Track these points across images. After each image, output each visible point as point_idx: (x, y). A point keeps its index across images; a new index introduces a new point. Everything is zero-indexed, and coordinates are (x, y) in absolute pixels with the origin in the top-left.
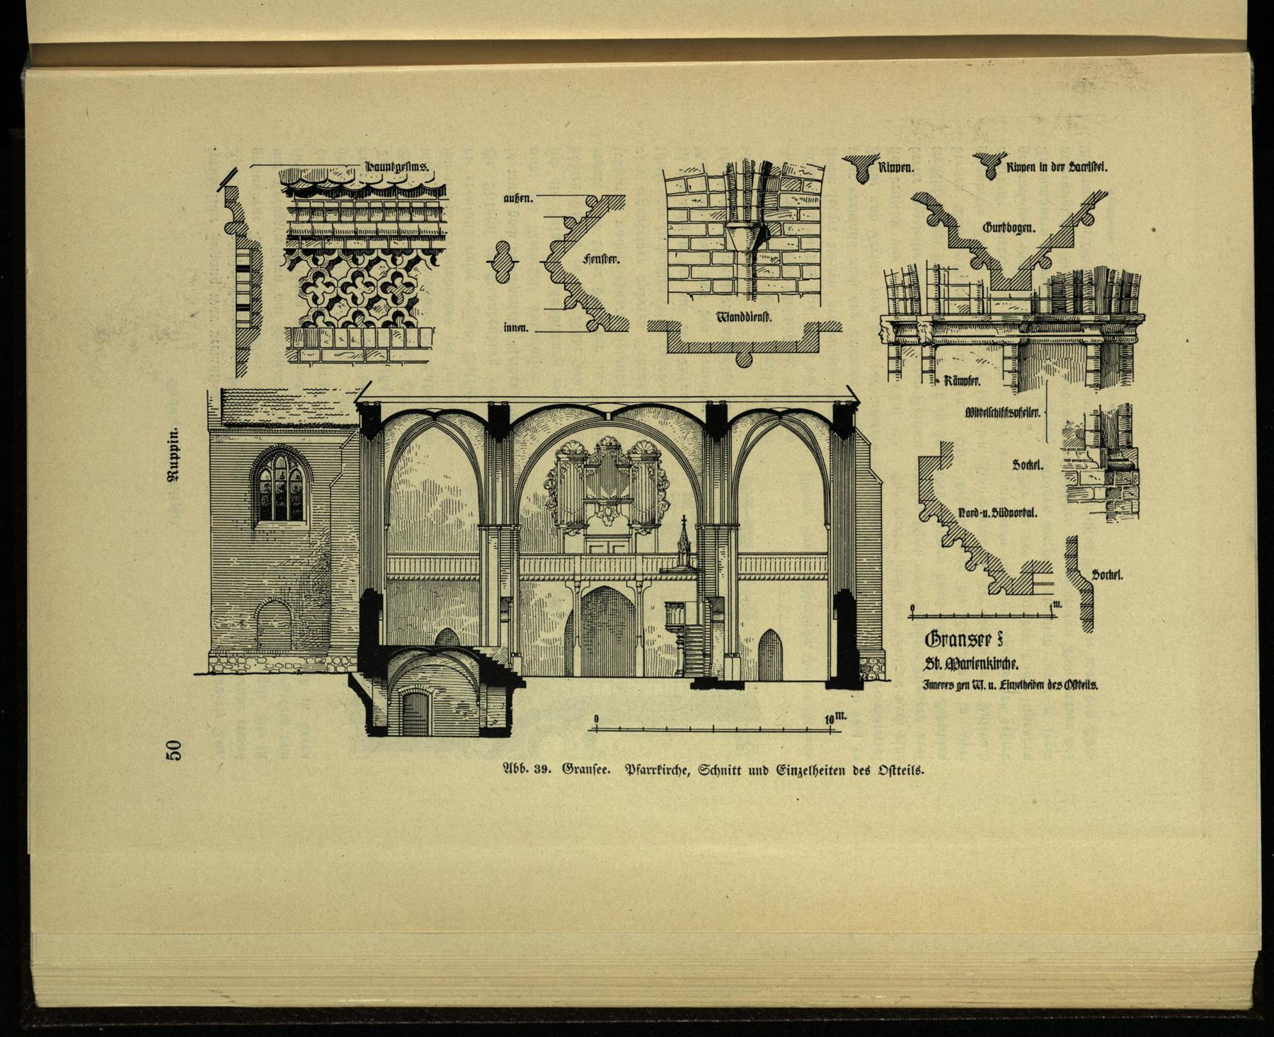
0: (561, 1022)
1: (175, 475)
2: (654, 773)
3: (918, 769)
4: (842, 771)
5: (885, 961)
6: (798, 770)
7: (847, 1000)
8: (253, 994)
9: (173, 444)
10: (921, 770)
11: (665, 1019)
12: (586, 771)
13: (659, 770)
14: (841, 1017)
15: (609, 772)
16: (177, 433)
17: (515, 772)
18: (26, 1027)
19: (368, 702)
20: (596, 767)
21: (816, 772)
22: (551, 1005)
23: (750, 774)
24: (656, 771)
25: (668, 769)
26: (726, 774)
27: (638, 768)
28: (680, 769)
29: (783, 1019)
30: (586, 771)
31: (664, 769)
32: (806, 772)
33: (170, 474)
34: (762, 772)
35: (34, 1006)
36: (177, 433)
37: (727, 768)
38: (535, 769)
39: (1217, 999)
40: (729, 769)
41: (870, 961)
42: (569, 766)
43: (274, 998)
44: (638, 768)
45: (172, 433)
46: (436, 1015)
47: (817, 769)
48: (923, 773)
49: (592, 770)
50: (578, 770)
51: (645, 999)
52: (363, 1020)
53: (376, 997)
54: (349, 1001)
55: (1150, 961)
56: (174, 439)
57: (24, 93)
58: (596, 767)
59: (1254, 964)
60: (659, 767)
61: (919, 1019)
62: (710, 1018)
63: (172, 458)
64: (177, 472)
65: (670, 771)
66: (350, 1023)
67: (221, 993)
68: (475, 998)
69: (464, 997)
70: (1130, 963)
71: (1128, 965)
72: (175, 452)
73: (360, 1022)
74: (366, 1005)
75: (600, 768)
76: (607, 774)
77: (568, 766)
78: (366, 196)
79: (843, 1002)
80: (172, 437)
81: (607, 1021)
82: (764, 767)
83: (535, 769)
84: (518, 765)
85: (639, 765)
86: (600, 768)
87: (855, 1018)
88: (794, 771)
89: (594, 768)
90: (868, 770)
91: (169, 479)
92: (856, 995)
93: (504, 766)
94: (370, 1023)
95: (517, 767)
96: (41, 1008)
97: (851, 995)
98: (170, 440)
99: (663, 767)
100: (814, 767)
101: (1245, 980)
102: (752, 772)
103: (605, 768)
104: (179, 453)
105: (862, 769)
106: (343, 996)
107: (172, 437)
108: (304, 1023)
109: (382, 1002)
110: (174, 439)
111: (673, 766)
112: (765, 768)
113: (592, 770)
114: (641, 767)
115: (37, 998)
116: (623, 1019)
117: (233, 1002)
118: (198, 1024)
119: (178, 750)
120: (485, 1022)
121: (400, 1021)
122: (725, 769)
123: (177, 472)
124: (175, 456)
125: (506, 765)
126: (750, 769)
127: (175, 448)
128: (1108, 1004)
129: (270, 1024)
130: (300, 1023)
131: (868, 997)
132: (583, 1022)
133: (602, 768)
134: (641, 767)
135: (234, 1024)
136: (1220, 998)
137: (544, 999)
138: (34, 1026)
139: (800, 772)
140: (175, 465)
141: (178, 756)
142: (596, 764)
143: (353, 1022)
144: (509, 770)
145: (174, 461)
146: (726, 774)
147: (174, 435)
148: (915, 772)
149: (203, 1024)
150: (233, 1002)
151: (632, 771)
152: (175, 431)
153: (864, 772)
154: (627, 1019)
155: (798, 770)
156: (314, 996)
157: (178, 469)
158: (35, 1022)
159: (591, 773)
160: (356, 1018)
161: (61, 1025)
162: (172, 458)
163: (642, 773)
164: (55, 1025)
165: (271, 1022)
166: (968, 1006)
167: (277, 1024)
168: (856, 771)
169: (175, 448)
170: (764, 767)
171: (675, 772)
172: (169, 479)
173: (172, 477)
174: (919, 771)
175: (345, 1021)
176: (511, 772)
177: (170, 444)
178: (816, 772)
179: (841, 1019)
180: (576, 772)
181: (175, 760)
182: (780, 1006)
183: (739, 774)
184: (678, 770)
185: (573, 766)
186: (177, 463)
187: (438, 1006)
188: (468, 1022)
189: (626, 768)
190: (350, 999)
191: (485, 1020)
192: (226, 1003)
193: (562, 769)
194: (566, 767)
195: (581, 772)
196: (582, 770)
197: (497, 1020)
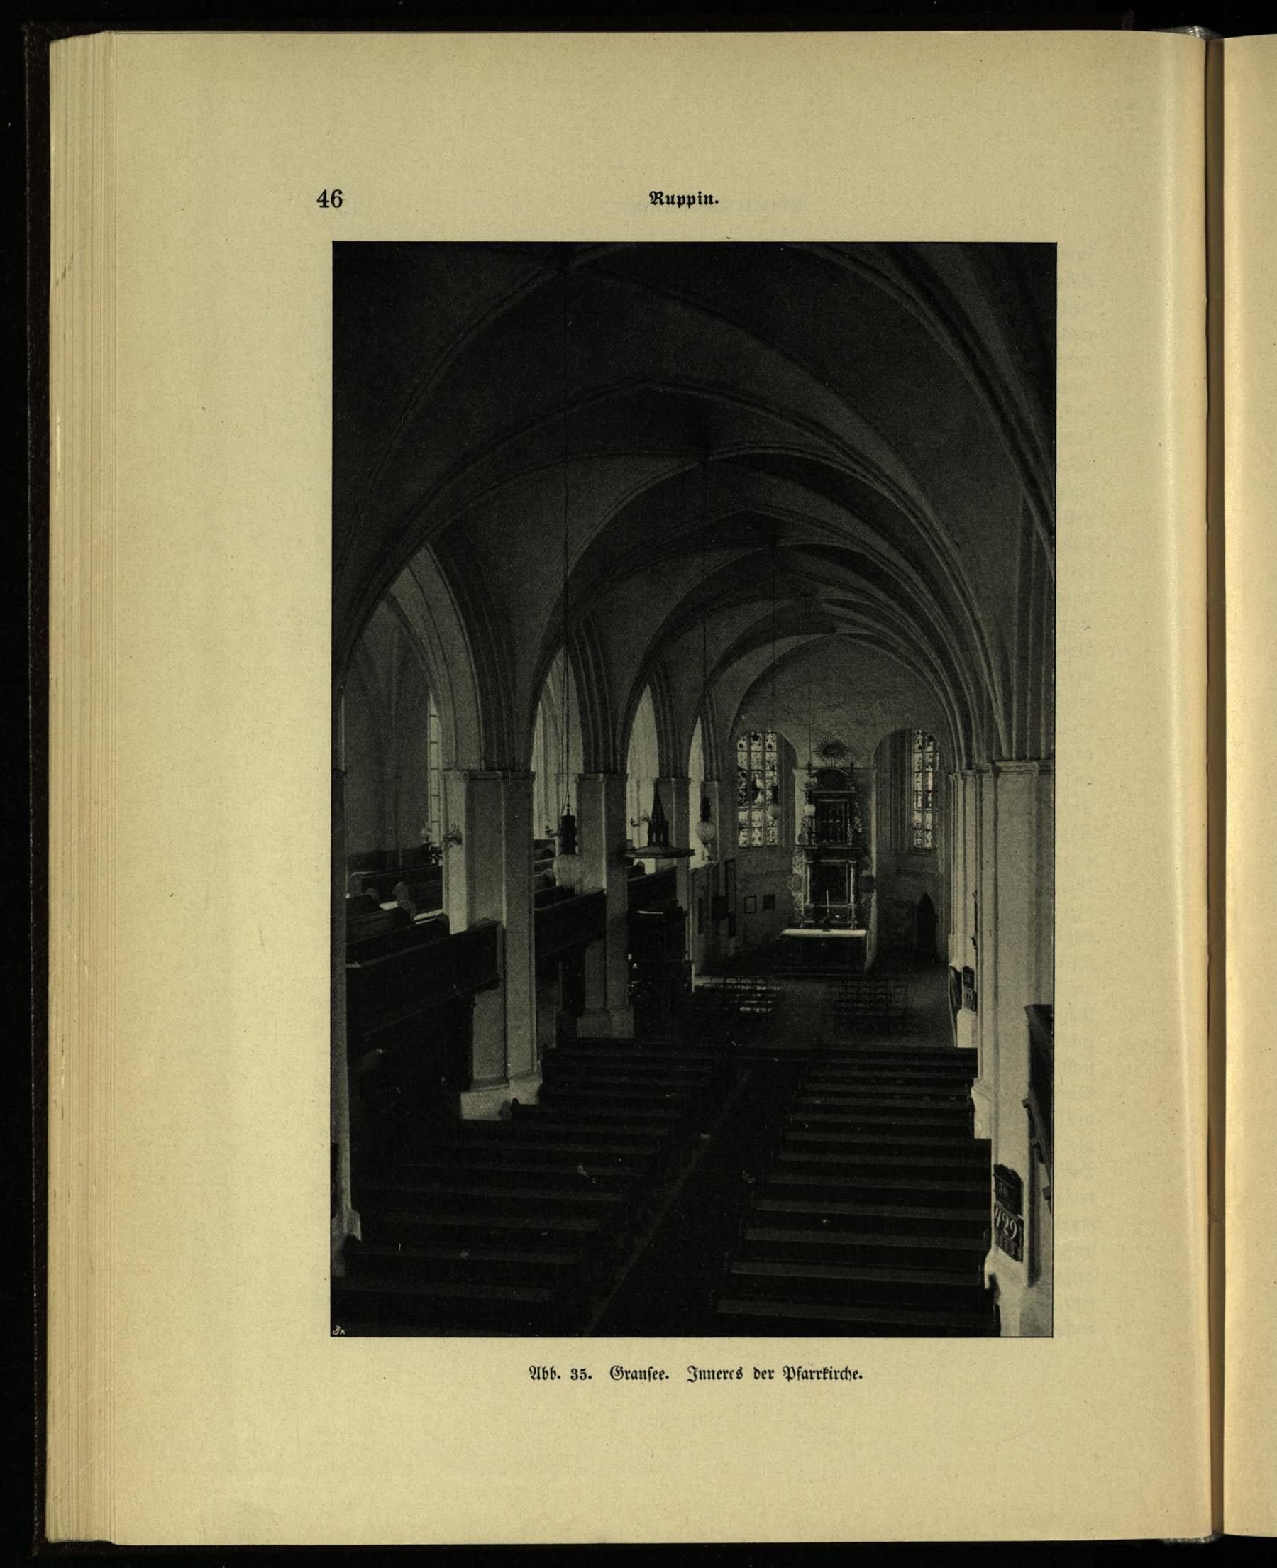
0: (30, 689)
1: (658, 200)
5: (113, 1086)
7: (59, 1040)
11: (34, 817)
12: (638, 1376)
13: (824, 1373)
14: (35, 1035)
16: (711, 203)
17: (544, 1378)
18: (24, 28)
20: (652, 1371)
22: (53, 675)
24: (821, 1375)
25: (835, 1372)
27: (799, 1372)
29: (34, 962)
30: (638, 1376)
31: (831, 1372)
33: (659, 195)
34: (638, 1374)
35: (52, 39)
36: (711, 203)
38: (571, 1374)
39: (59, 1498)
41: (113, 1067)
42: (619, 1369)
43: (62, 334)
44: (799, 1372)
45: (711, 197)
46: (40, 534)
49: (647, 1374)
50: (629, 1375)
51: (60, 792)
52: (33, 444)
53: (64, 458)
54: (58, 427)
55: (112, 1412)
56: (703, 200)
58: (652, 1371)
59: (108, 1540)
61: (33, 1131)
62: (35, 872)
63: (679, 197)
64: (662, 203)
65: (838, 1375)
66: (30, 428)
67: (70, 268)
68: (61, 581)
69: (64, 568)
70: (111, 1386)
71: (108, 1385)
72: (687, 201)
73: (30, 442)
74: (52, 448)
75: (656, 1372)
79: (56, 1035)
80: (706, 197)
81: (31, 746)
83: (571, 1374)
84: (548, 1369)
85: (800, 1367)
86: (656, 1372)
87: (35, 1052)
89: (649, 1372)
90: (740, 1373)
91: (653, 194)
92: (66, 1052)
94: (29, 454)
95: (547, 1372)
96: (48, 48)
97: (66, 1046)
98: (702, 195)
99: (829, 1369)
101: (86, 1529)
104: (685, 207)
106: (64, 417)
107: (706, 197)
108: (29, 372)
109: (56, 468)
110: (703, 200)
113: (647, 1374)
114: (802, 1370)
115: (62, 42)
116: (34, 766)
117: (57, 283)
118: (29, 241)
120: (30, 595)
121: (31, 490)
123: (662, 203)
124: (682, 202)
125: (532, 1369)
127: (692, 201)
128: (53, 1363)
129: (28, 330)
130: (29, 366)
131: (63, 1067)
132: (30, 716)
133: (659, 1372)
134: (802, 1370)
135: (28, 286)
136: (61, 1500)
137: (60, 667)
138: (26, 38)
140: (670, 201)
142: (651, 1367)
143: (30, 433)
144: (536, 1376)
145: (676, 200)
147: (709, 200)
149: (28, 246)
150: (57, 283)
151: (792, 1375)
154: (34, 771)
156: (65, 383)
158: (31, 40)
160: (36, 436)
161: (27, 72)
162: (679, 197)
163: (803, 1378)
164: (27, 65)
165: (30, 331)
166: (50, 1192)
167: (28, 339)
169: (690, 201)
172: (653, 194)
173: (656, 197)
175: (32, 423)
176: (539, 1378)
177: (697, 195)
179: (33, 1034)
180: (627, 1378)
182: (51, 959)
185: (624, 1370)
186: (673, 203)
187: (50, 537)
188: (30, 574)
189: (784, 1371)
190: (61, 427)
191: (32, 595)
192: (55, 273)
194: (614, 1371)
196: (634, 1375)
197: (33, 610)
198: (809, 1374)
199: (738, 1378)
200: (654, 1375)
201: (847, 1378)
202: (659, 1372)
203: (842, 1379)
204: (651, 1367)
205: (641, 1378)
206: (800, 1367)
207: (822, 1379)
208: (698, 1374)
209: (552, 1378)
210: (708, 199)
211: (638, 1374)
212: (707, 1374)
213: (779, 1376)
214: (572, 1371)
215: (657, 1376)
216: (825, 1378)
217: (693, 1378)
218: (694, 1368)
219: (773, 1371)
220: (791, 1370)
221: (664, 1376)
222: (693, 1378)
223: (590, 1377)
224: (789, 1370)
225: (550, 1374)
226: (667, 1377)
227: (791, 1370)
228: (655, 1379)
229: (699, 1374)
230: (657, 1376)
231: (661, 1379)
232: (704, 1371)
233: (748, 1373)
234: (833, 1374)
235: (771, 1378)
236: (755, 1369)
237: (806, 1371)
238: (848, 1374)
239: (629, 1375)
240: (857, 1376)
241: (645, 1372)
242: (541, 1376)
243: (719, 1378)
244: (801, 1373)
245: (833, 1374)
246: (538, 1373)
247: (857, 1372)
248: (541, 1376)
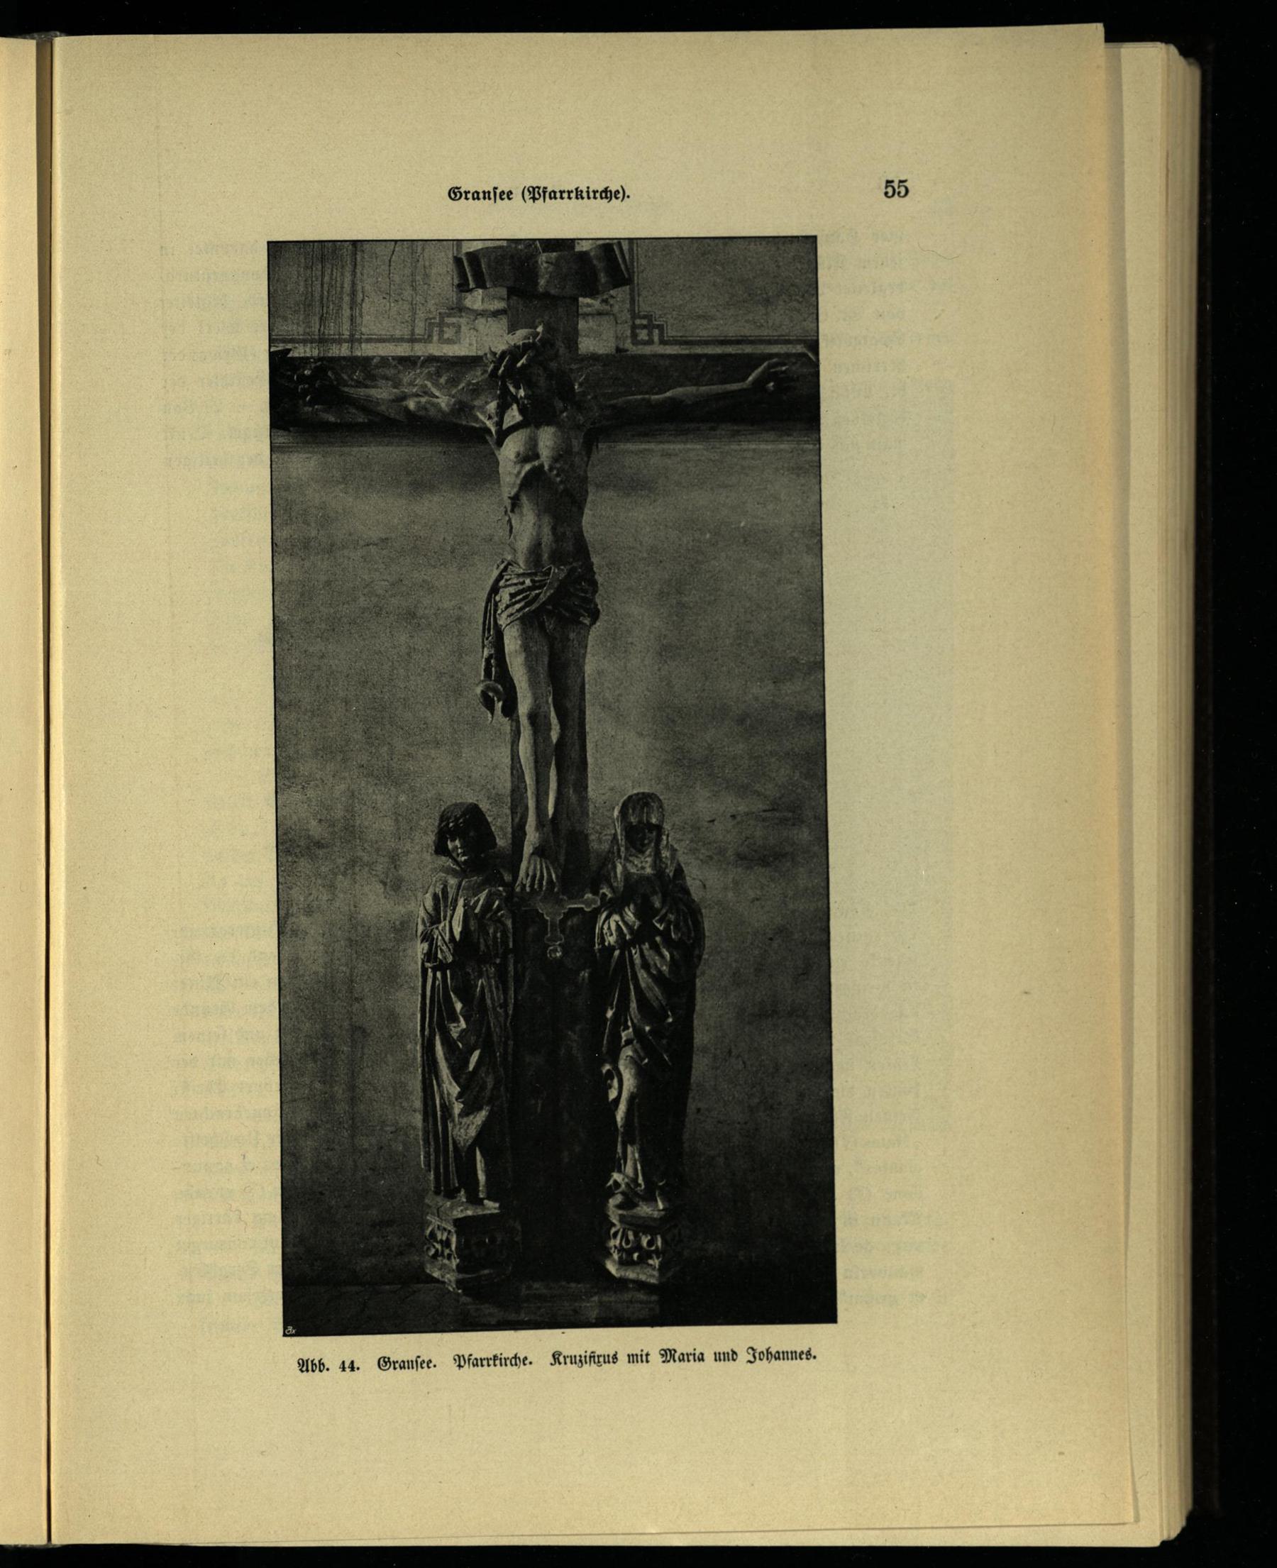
2: (489, 1365)
3: (809, 1353)
4: (701, 1358)
6: (578, 1358)
10: (813, 1353)
13: (494, 1360)
15: (435, 1366)
17: (313, 1371)
20: (419, 1360)
21: (770, 1356)
23: (716, 1360)
24: (491, 1362)
25: (505, 1359)
26: (642, 1361)
27: (469, 1360)
31: (501, 1359)
34: (406, 1364)
37: (583, 1354)
40: (641, 1355)
42: (386, 1360)
44: (469, 1360)
47: (771, 1353)
48: (815, 1357)
49: (414, 1363)
50: (397, 1365)
56: (591, 195)
57: (25, 38)
58: (419, 1360)
60: (495, 1357)
65: (508, 1362)
75: (424, 1361)
76: (528, 1365)
77: (384, 1361)
80: (490, 199)
82: (732, 1351)
84: (316, 1362)
85: (471, 1355)
86: (424, 1361)
88: (574, 1360)
89: (417, 1362)
90: (615, 1357)
93: (299, 1363)
98: (591, 190)
99: (499, 1357)
100: (312, 1361)
102: (718, 1357)
103: (430, 1361)
105: (802, 1352)
110: (591, 195)
112: (734, 1353)
113: (414, 1363)
119: (896, 195)
122: (637, 1355)
125: (301, 1361)
126: (715, 1354)
133: (805, 1352)
134: (473, 1358)
139: (581, 1361)
141: (890, 194)
142: (419, 1357)
144: (304, 1369)
146: (637, 1362)
148: (611, 1360)
151: (462, 1363)
153: (804, 1356)
155: (578, 1358)
157: (592, 199)
159: (413, 1368)
163: (474, 1366)
170: (732, 1351)
172: (531, 189)
173: (455, 193)
174: (810, 1355)
176: (307, 1370)
178: (770, 1356)
180: (395, 1368)
181: (884, 191)
183: (647, 1361)
184: (518, 1360)
185: (391, 1360)
189: (455, 1360)
193: (376, 1363)
194: (382, 1362)
195: (401, 1368)
196: (402, 1364)
198: (686, 1357)
199: (614, 1363)
200: (421, 1364)
201: (516, 1365)
202: (805, 1352)
203: (512, 1365)
204: (419, 1357)
205: (784, 1359)
206: (471, 1355)
207: (492, 1366)
208: (757, 1355)
209: (321, 1371)
211: (406, 1364)
212: (790, 1355)
213: (656, 1358)
214: (554, 1356)
215: (425, 1365)
216: (495, 1365)
217: (752, 1359)
218: (753, 1349)
220: (462, 1359)
221: (431, 1365)
222: (752, 1359)
223: (328, 1369)
224: (459, 1357)
225: (320, 1367)
227: (462, 1359)
228: (422, 1368)
229: (460, 1361)
230: (425, 1365)
232: (787, 1352)
233: (622, 1358)
234: (503, 1361)
237: (476, 1359)
238: (517, 1360)
239: (397, 1365)
240: (527, 1362)
241: (412, 1361)
242: (310, 1368)
243: (422, 1368)
244: (471, 1361)
245: (503, 1361)
246: (304, 1365)
247: (430, 1361)
248: (310, 1368)
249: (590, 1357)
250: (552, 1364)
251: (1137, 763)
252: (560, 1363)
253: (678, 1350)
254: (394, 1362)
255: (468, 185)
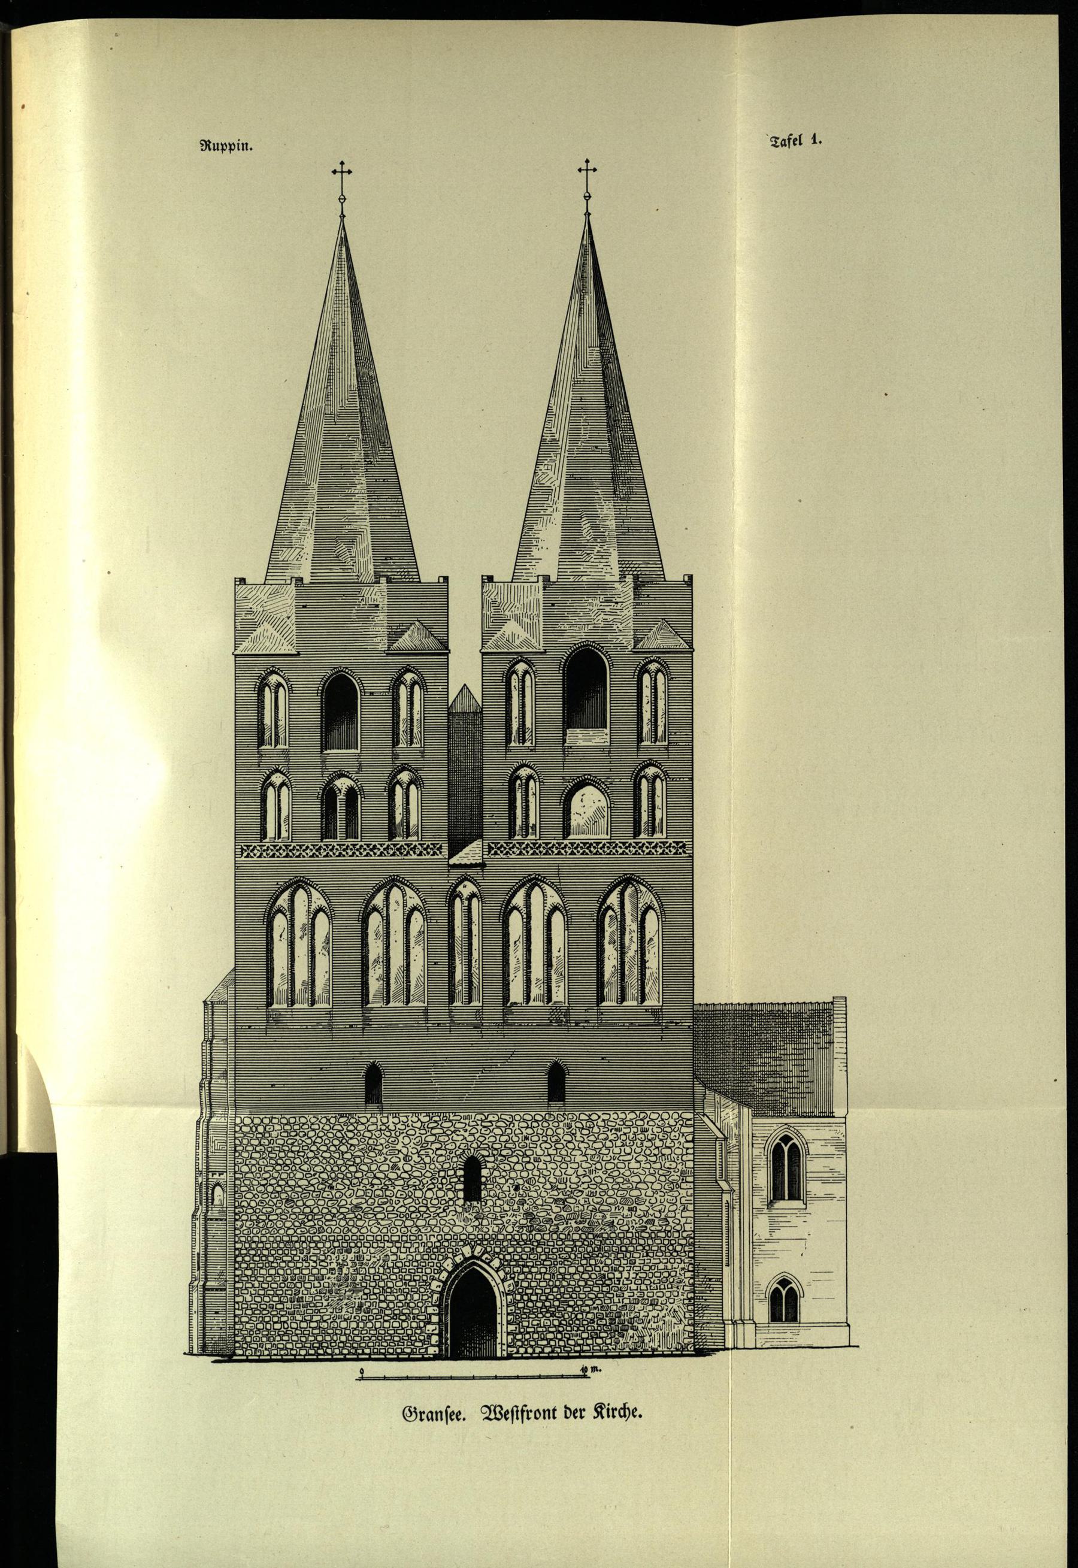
8: (197, 1222)
9: (236, 146)
19: (202, 1113)
20: (449, 1410)
25: (613, 1409)
26: (549, 1418)
28: (628, 1409)
31: (608, 1409)
32: (453, 1417)
42: (412, 1410)
44: (523, 1411)
45: (247, 144)
50: (424, 1416)
58: (449, 1410)
65: (616, 1413)
75: (453, 1412)
77: (409, 1410)
78: (326, 750)
86: (453, 1412)
89: (446, 1411)
111: (619, 1406)
133: (456, 1412)
142: (448, 1407)
147: (245, 146)
151: (568, 1415)
152: (249, 148)
159: (442, 1419)
168: (568, 1411)
171: (622, 1414)
173: (206, 144)
180: (421, 1420)
183: (554, 1418)
184: (627, 1411)
185: (418, 1411)
194: (407, 1411)
196: (430, 1415)
200: (451, 1416)
201: (625, 1416)
202: (456, 1412)
204: (448, 1407)
210: (216, 148)
214: (596, 1410)
215: (454, 1417)
219: (584, 1410)
226: (464, 1419)
228: (452, 1420)
230: (454, 1417)
231: (458, 1420)
234: (611, 1411)
235: (582, 1417)
236: (566, 1407)
238: (453, 1416)
239: (424, 1416)
241: (441, 1412)
243: (528, 1418)
245: (611, 1411)
247: (636, 1409)
249: (523, 1411)
250: (595, 1418)
251: (626, 912)
252: (602, 1417)
253: (503, 1407)
254: (420, 1413)
255: (215, 140)
